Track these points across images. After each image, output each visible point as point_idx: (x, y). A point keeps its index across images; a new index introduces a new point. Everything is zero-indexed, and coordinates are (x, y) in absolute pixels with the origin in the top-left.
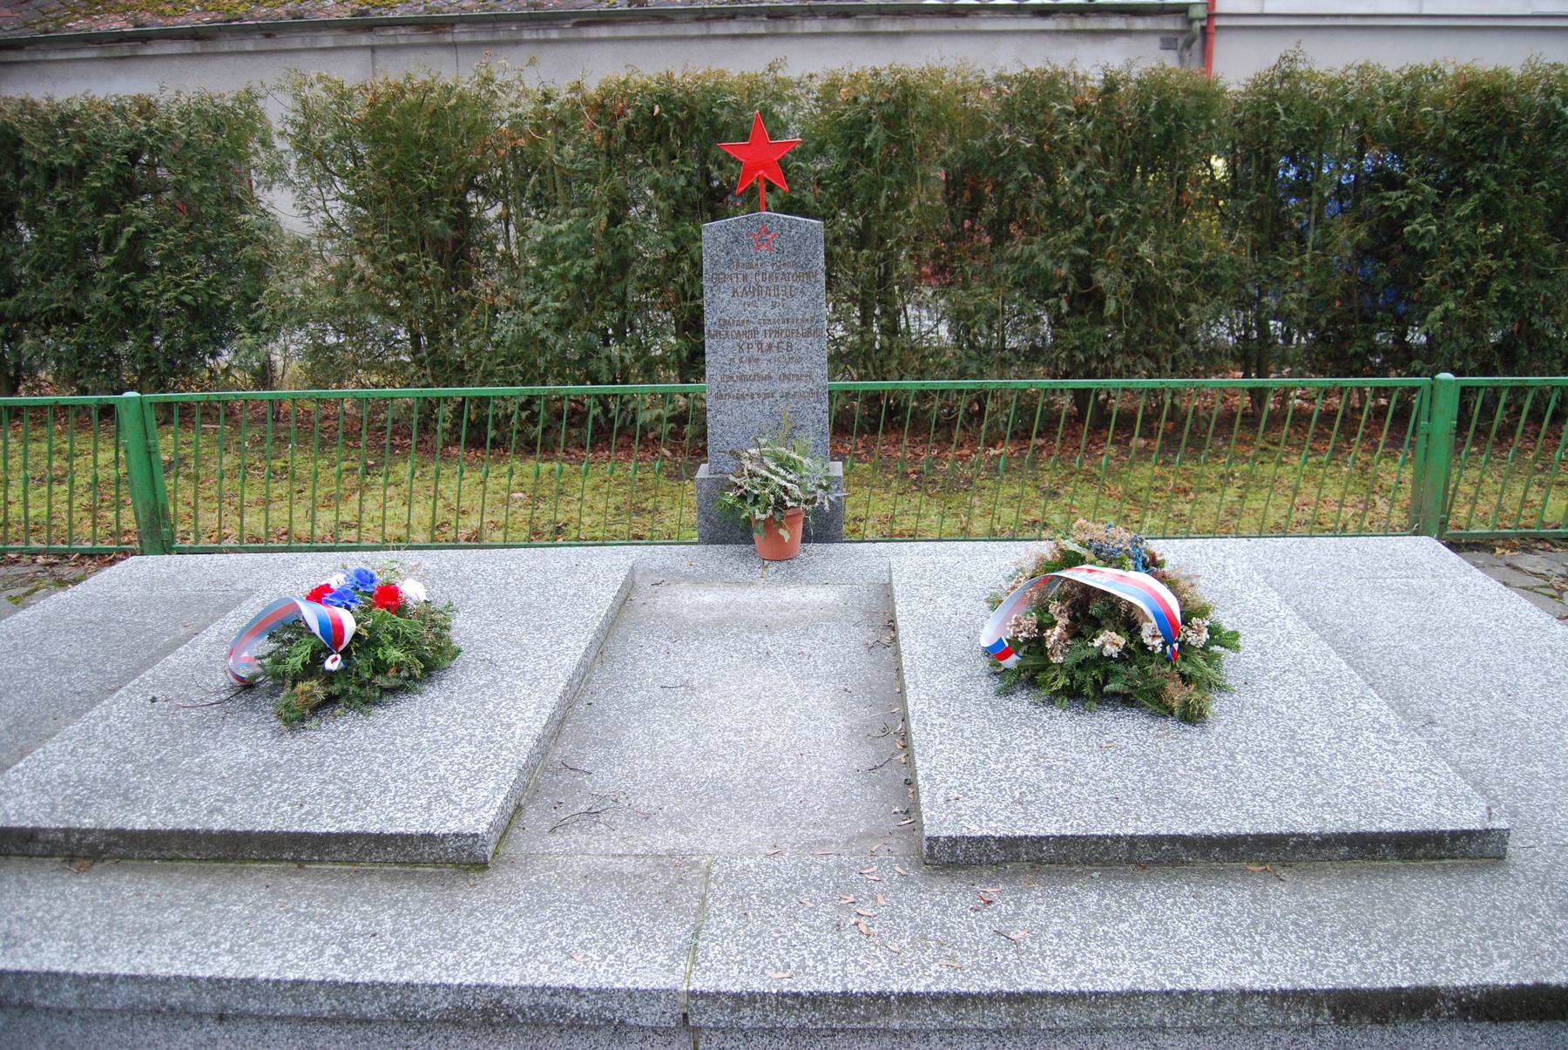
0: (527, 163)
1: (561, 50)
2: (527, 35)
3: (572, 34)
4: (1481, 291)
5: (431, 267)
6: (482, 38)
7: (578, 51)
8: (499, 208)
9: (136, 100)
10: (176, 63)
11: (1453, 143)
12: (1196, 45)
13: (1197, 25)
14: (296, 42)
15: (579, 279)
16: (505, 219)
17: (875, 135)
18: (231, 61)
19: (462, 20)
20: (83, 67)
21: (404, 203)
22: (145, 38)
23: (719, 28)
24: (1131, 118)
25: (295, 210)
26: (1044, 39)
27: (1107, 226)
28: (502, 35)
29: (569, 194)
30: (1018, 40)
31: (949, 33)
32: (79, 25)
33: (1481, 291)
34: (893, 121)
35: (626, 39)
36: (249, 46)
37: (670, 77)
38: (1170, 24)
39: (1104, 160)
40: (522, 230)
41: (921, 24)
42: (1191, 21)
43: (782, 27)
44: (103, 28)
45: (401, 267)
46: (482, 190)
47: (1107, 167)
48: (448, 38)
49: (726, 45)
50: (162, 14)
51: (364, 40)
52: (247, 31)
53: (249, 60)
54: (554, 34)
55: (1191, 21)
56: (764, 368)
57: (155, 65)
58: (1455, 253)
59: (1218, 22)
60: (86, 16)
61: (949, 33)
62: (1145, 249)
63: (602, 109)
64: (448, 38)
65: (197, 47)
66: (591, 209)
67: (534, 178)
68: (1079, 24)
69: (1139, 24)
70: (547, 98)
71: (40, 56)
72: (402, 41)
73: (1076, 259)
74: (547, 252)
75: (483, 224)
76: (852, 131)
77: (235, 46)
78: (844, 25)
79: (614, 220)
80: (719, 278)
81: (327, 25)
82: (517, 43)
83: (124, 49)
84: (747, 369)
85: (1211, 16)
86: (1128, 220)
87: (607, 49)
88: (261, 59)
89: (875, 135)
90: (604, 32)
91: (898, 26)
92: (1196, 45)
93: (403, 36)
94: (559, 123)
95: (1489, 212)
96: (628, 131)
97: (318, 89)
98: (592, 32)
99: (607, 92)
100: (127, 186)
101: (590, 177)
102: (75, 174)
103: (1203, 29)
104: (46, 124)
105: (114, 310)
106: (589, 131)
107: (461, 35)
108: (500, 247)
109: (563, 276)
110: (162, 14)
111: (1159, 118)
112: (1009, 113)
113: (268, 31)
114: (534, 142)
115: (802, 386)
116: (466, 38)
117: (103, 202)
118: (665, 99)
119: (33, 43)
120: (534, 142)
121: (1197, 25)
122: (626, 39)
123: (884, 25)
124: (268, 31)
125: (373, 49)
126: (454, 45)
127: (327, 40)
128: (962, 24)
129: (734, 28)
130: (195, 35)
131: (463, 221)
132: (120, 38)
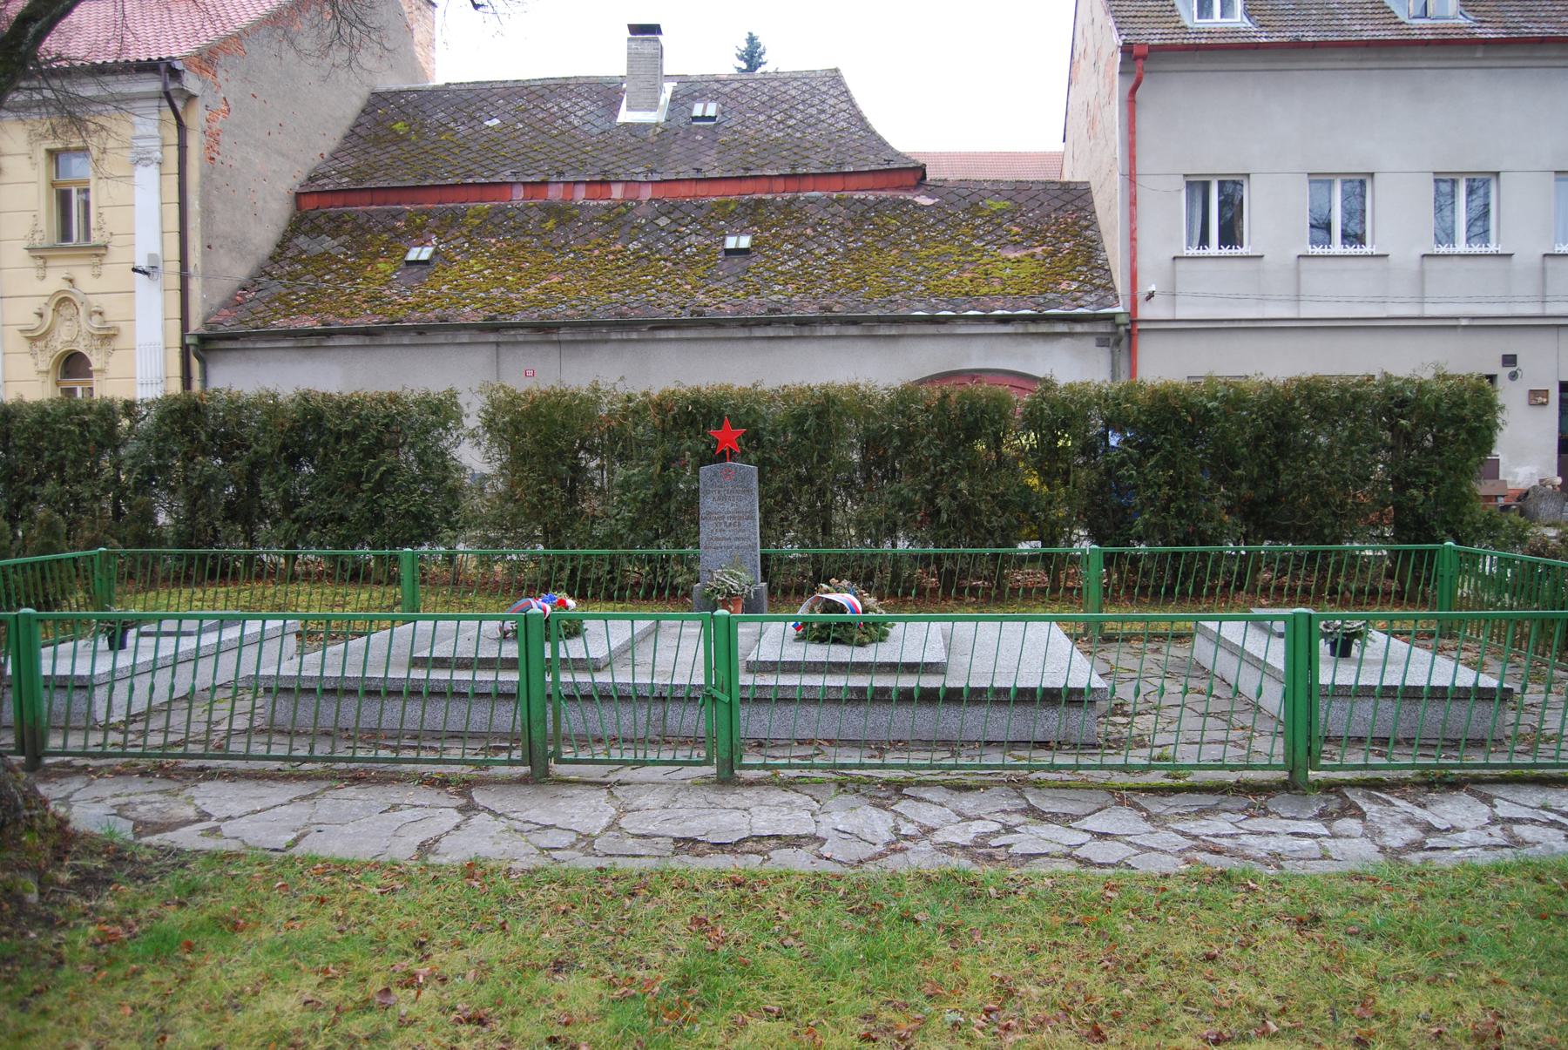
0: (616, 435)
1: (640, 347)
2: (614, 336)
3: (648, 336)
4: (1166, 509)
5: (557, 492)
6: (579, 337)
7: (652, 347)
8: (598, 461)
9: (390, 394)
10: (350, 351)
11: (1145, 424)
12: (1124, 343)
13: (1122, 329)
14: (441, 339)
15: (643, 501)
16: (601, 467)
17: (810, 422)
18: (391, 350)
19: (566, 325)
20: (281, 353)
21: (547, 457)
22: (329, 334)
23: (758, 332)
24: (955, 411)
25: (474, 458)
26: (1006, 340)
27: (942, 473)
28: (595, 336)
29: (639, 453)
30: (986, 341)
31: (934, 336)
32: (280, 323)
33: (1166, 509)
34: (819, 415)
35: (688, 340)
36: (406, 340)
37: (698, 390)
38: (1102, 328)
39: (940, 436)
40: (611, 472)
41: (911, 329)
42: (1118, 326)
43: (806, 331)
44: (299, 326)
45: (542, 492)
46: (588, 451)
47: (942, 440)
48: (555, 337)
49: (765, 344)
50: (342, 316)
51: (492, 337)
52: (406, 330)
53: (404, 350)
54: (634, 336)
55: (1118, 326)
56: (727, 534)
57: (332, 353)
58: (1148, 486)
59: (1140, 326)
60: (285, 316)
61: (934, 336)
62: (962, 485)
63: (661, 406)
64: (555, 337)
65: (367, 340)
66: (652, 462)
67: (619, 444)
68: (1032, 328)
69: (1078, 328)
70: (629, 400)
71: (250, 345)
72: (520, 339)
73: (925, 492)
74: (626, 486)
75: (585, 469)
76: (800, 419)
77: (395, 341)
78: (853, 330)
79: (664, 468)
80: (707, 492)
81: (465, 327)
82: (607, 341)
83: (313, 341)
84: (719, 535)
85: (1133, 322)
86: (954, 470)
87: (673, 347)
88: (414, 350)
89: (810, 422)
90: (672, 334)
91: (894, 331)
92: (1124, 343)
93: (521, 335)
94: (636, 412)
95: (1168, 462)
96: (674, 419)
97: (502, 394)
98: (663, 334)
99: (663, 398)
100: (378, 445)
101: (652, 444)
102: (353, 436)
103: (1128, 331)
104: (339, 407)
105: (368, 515)
106: (653, 418)
107: (565, 335)
108: (597, 484)
109: (634, 499)
110: (342, 316)
111: (971, 411)
112: (891, 409)
113: (421, 330)
114: (621, 424)
115: (745, 543)
116: (568, 337)
117: (369, 452)
118: (695, 402)
119: (247, 335)
120: (621, 424)
121: (1122, 329)
122: (688, 340)
123: (883, 330)
124: (421, 330)
125: (498, 344)
126: (559, 342)
127: (464, 337)
128: (943, 329)
129: (770, 332)
130: (367, 332)
131: (577, 470)
132: (311, 333)
